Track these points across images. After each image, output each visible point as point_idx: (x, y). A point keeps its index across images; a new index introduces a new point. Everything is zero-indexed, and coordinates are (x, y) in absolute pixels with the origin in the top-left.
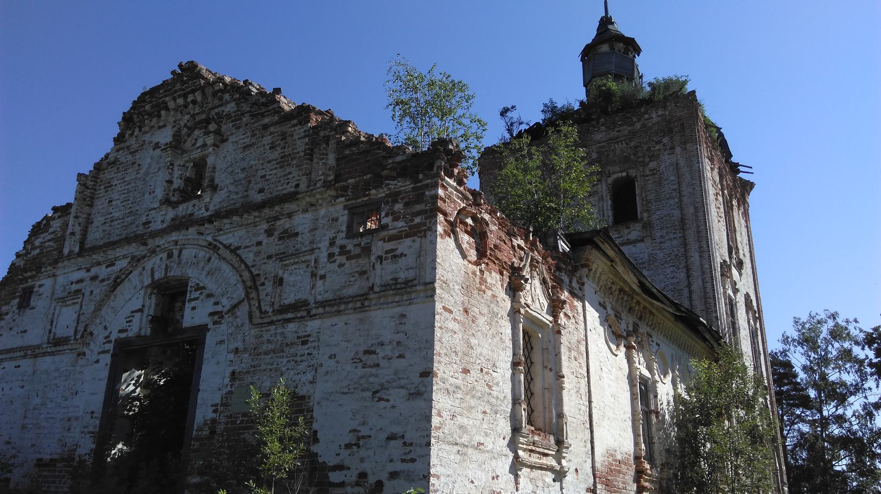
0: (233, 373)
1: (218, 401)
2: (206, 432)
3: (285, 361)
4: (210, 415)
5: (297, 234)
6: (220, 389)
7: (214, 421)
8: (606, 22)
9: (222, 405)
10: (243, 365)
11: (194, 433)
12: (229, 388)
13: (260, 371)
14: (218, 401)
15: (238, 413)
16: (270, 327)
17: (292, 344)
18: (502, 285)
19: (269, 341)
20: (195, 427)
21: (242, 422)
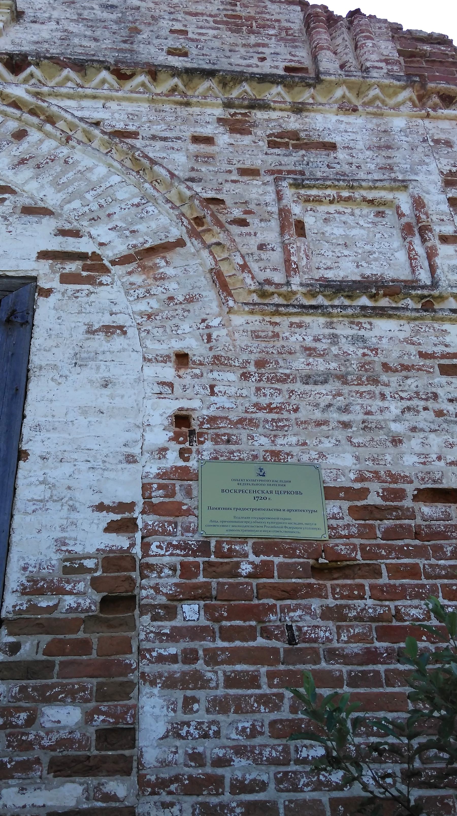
0: (181, 420)
1: (132, 493)
2: (81, 598)
3: (395, 408)
4: (93, 538)
5: (332, 147)
6: (131, 459)
7: (115, 561)
8: (305, 237)
9: (150, 508)
10: (220, 400)
11: (11, 601)
12: (172, 459)
13: (299, 423)
14: (132, 493)
15: (244, 540)
16: (307, 319)
17: (405, 368)
18: (199, 774)
19: (310, 351)
20: (15, 577)
21: (263, 570)
